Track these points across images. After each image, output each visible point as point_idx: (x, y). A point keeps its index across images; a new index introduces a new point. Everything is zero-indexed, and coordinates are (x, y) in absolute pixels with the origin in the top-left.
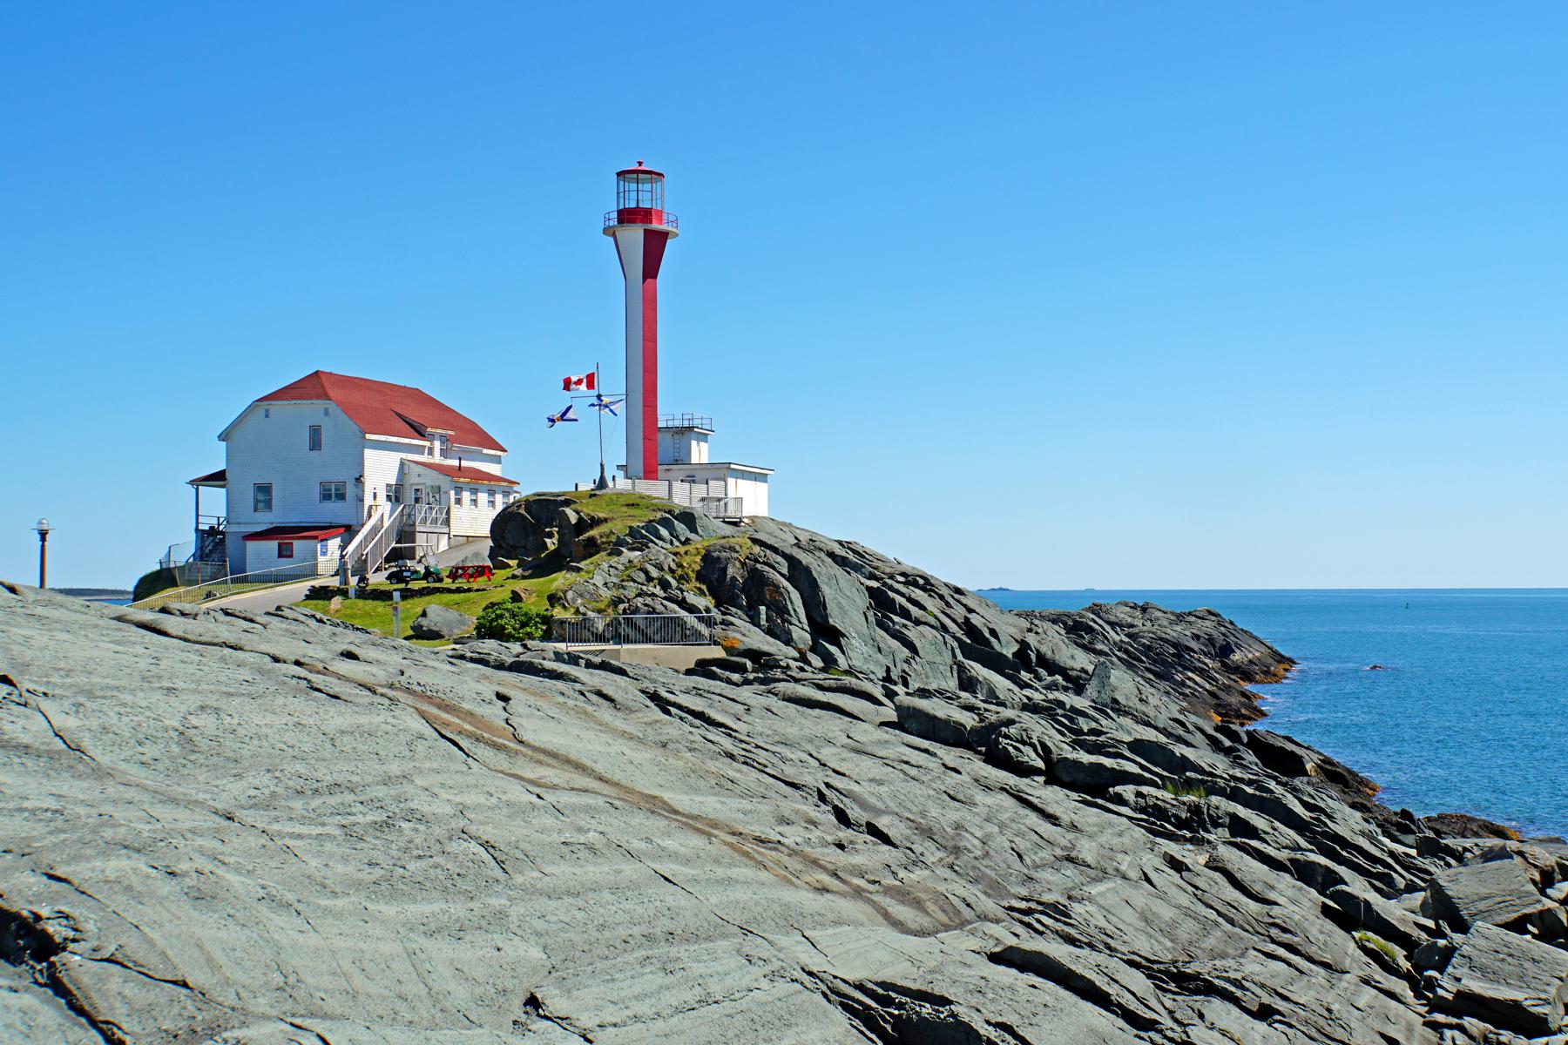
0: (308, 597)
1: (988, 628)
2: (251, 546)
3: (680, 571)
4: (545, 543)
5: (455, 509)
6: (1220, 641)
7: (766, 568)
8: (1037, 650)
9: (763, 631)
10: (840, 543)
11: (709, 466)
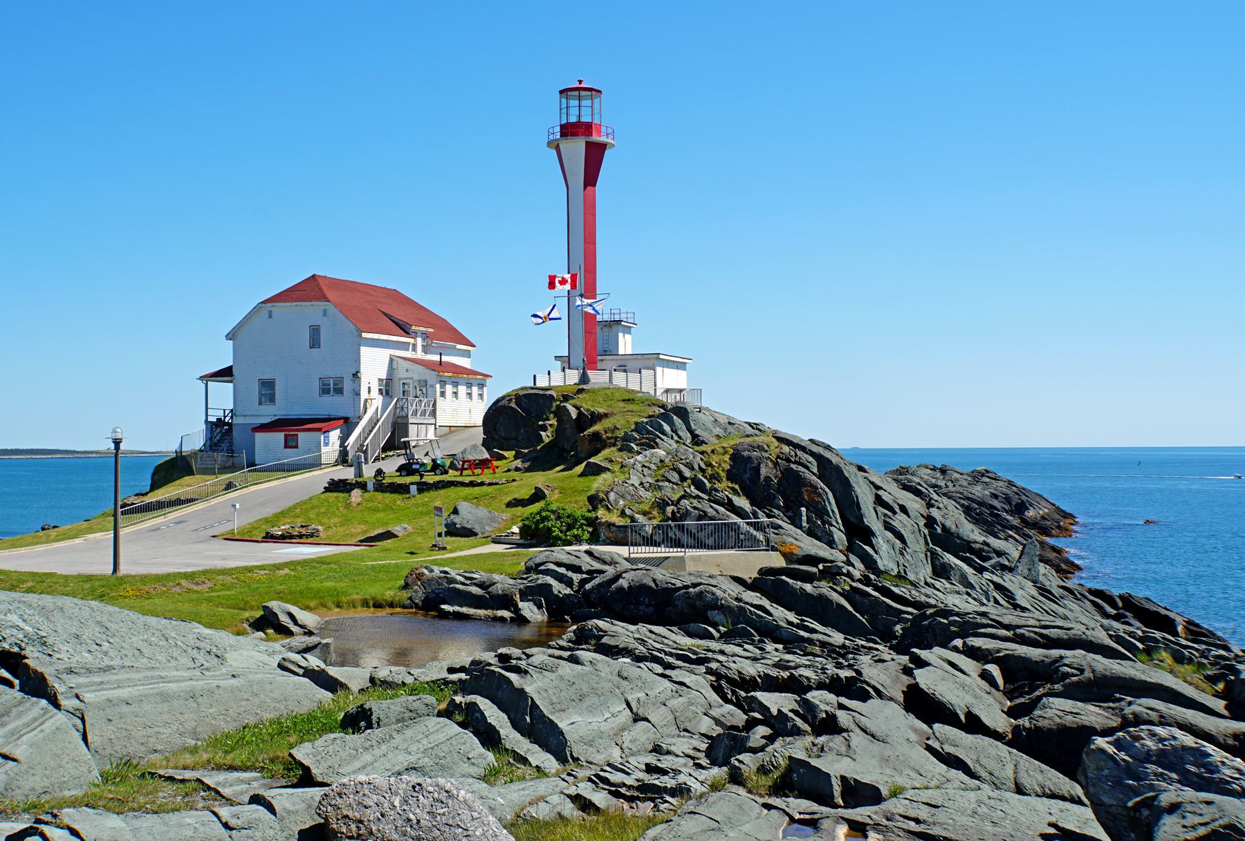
0: (327, 490)
1: (898, 504)
2: (259, 436)
3: (709, 471)
5: (440, 401)
6: (1015, 500)
7: (801, 469)
8: (943, 525)
9: (804, 532)
10: (749, 424)
11: (640, 357)
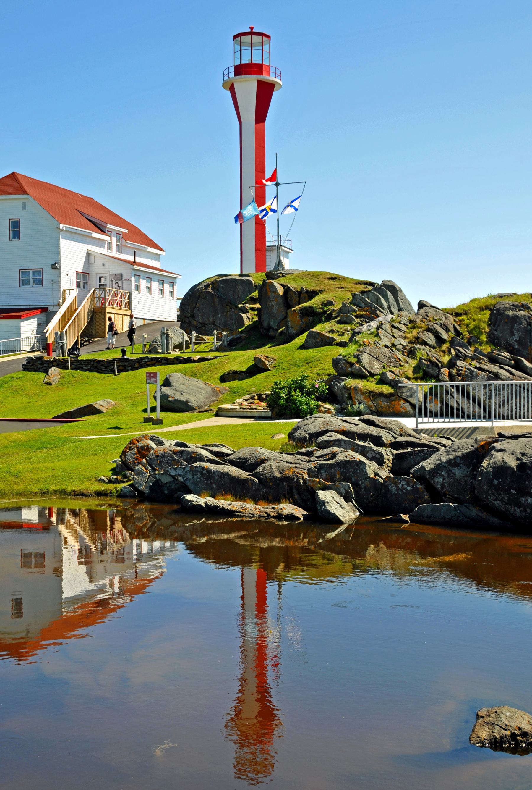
4: (242, 317)
5: (135, 295)
